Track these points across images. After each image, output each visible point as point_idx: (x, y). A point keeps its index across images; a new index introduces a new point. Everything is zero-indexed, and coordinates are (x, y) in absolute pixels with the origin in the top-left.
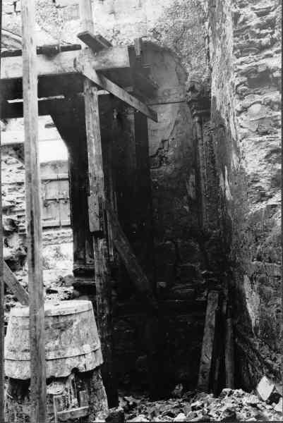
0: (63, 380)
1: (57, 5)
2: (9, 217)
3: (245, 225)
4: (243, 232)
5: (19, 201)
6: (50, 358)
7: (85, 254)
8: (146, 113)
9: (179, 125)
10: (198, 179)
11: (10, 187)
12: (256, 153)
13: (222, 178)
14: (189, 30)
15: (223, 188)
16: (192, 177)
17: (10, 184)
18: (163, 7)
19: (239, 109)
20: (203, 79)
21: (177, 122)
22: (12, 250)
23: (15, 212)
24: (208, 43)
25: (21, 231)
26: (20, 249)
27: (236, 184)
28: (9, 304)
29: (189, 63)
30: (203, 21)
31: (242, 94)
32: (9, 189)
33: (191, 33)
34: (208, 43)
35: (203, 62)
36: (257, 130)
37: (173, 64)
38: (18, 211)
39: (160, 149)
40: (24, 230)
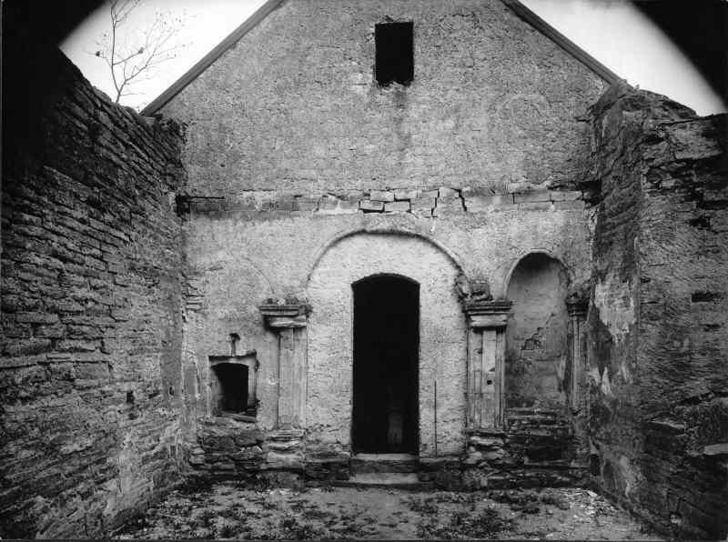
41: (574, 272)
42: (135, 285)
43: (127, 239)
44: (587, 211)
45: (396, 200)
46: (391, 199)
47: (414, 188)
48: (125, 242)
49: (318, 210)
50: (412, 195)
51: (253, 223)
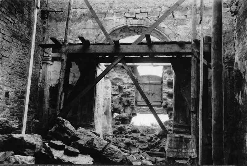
0: (187, 159)
1: (175, 19)
2: (127, 99)
5: (132, 92)
6: (183, 151)
7: (179, 119)
11: (128, 85)
15: (237, 99)
17: (128, 84)
20: (232, 54)
22: (127, 114)
23: (130, 97)
24: (235, 39)
25: (131, 106)
26: (130, 114)
28: (123, 139)
30: (233, 31)
32: (128, 86)
33: (228, 35)
34: (235, 39)
35: (232, 47)
38: (131, 97)
40: (133, 106)
41: (226, 47)
42: (15, 43)
43: (13, 22)
44: (233, 18)
45: (141, 12)
46: (139, 12)
47: (150, 7)
48: (11, 22)
49: (105, 17)
50: (149, 10)
51: (76, 23)
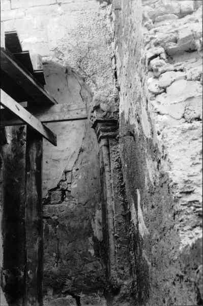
3: (174, 270)
4: (168, 284)
8: (41, 131)
9: (84, 154)
10: (105, 218)
12: (185, 147)
13: (133, 210)
14: (95, 51)
16: (99, 213)
18: (66, 28)
19: (155, 90)
21: (81, 150)
27: (153, 207)
29: (94, 82)
31: (157, 70)
36: (183, 117)
37: (78, 87)
39: (62, 181)
